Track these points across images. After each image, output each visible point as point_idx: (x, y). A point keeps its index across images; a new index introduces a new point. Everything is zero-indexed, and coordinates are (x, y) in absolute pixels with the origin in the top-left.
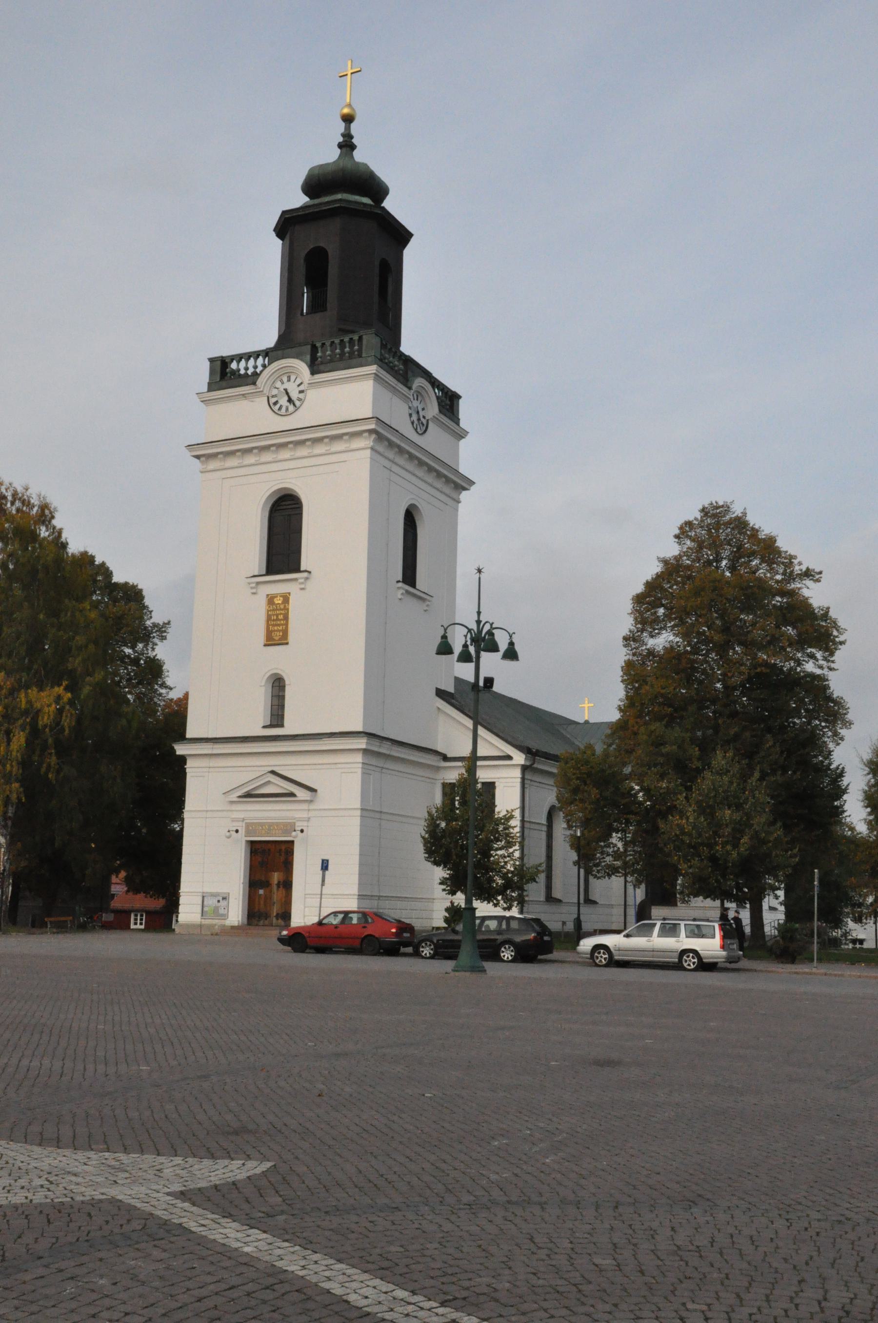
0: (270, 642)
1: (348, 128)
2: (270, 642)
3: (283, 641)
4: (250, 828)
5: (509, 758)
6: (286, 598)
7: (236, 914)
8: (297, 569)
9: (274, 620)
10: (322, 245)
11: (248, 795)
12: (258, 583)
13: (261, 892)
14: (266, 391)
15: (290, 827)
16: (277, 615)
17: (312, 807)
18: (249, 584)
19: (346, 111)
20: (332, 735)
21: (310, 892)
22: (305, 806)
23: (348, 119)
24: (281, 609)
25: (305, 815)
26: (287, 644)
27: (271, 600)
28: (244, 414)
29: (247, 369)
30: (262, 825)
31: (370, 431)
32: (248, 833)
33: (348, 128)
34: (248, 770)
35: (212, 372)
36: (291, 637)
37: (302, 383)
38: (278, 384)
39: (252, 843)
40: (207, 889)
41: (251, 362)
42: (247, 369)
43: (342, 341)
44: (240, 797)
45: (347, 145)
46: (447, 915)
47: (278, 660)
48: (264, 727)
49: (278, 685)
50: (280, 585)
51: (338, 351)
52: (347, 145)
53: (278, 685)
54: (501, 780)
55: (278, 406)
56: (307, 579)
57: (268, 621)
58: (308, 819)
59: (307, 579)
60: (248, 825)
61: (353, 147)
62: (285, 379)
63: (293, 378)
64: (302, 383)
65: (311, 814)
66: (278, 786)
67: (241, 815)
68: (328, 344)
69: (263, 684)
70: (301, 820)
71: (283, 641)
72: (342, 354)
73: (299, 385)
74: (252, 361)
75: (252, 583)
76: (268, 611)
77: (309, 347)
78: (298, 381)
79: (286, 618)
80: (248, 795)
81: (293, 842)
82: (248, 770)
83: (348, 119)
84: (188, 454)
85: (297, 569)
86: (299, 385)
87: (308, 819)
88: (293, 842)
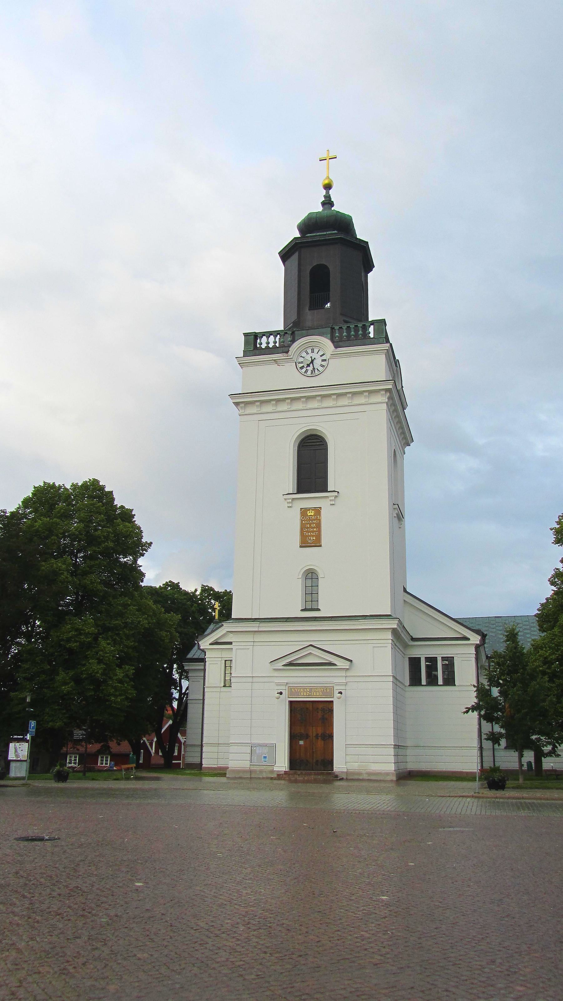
0: (304, 544)
1: (328, 193)
2: (304, 544)
3: (317, 544)
4: (292, 691)
5: (467, 639)
6: (318, 511)
7: (282, 763)
8: (324, 488)
9: (308, 528)
10: (324, 262)
11: (290, 664)
12: (293, 499)
13: (301, 743)
14: (295, 359)
15: (329, 691)
16: (310, 525)
17: (349, 674)
18: (286, 499)
19: (326, 182)
20: (365, 617)
21: (349, 743)
22: (343, 673)
23: (328, 187)
24: (314, 520)
25: (343, 680)
26: (321, 546)
27: (304, 512)
28: (278, 374)
29: (268, 343)
30: (304, 688)
31: (387, 390)
32: (291, 694)
33: (328, 193)
34: (287, 644)
35: (246, 343)
36: (323, 542)
37: (324, 354)
38: (304, 354)
39: (291, 702)
40: (255, 741)
41: (272, 338)
42: (268, 343)
43: (356, 326)
44: (284, 665)
45: (328, 203)
46: (543, 758)
47: (311, 557)
48: (302, 610)
49: (311, 576)
50: (311, 500)
51: (360, 332)
52: (328, 203)
53: (311, 576)
54: (459, 656)
55: (323, 363)
56: (336, 497)
57: (302, 529)
58: (346, 684)
59: (336, 497)
60: (290, 689)
61: (332, 204)
62: (309, 351)
63: (316, 350)
64: (324, 354)
65: (349, 679)
66: (318, 657)
67: (285, 680)
68: (344, 328)
69: (300, 577)
70: (339, 684)
71: (317, 544)
72: (349, 336)
73: (321, 356)
74: (272, 337)
75: (289, 499)
76: (302, 521)
77: (329, 329)
78: (321, 353)
79: (319, 526)
80: (290, 664)
81: (333, 701)
82: (287, 644)
83: (328, 187)
84: (231, 401)
85: (324, 488)
86: (321, 356)
87: (346, 684)
88: (333, 701)
